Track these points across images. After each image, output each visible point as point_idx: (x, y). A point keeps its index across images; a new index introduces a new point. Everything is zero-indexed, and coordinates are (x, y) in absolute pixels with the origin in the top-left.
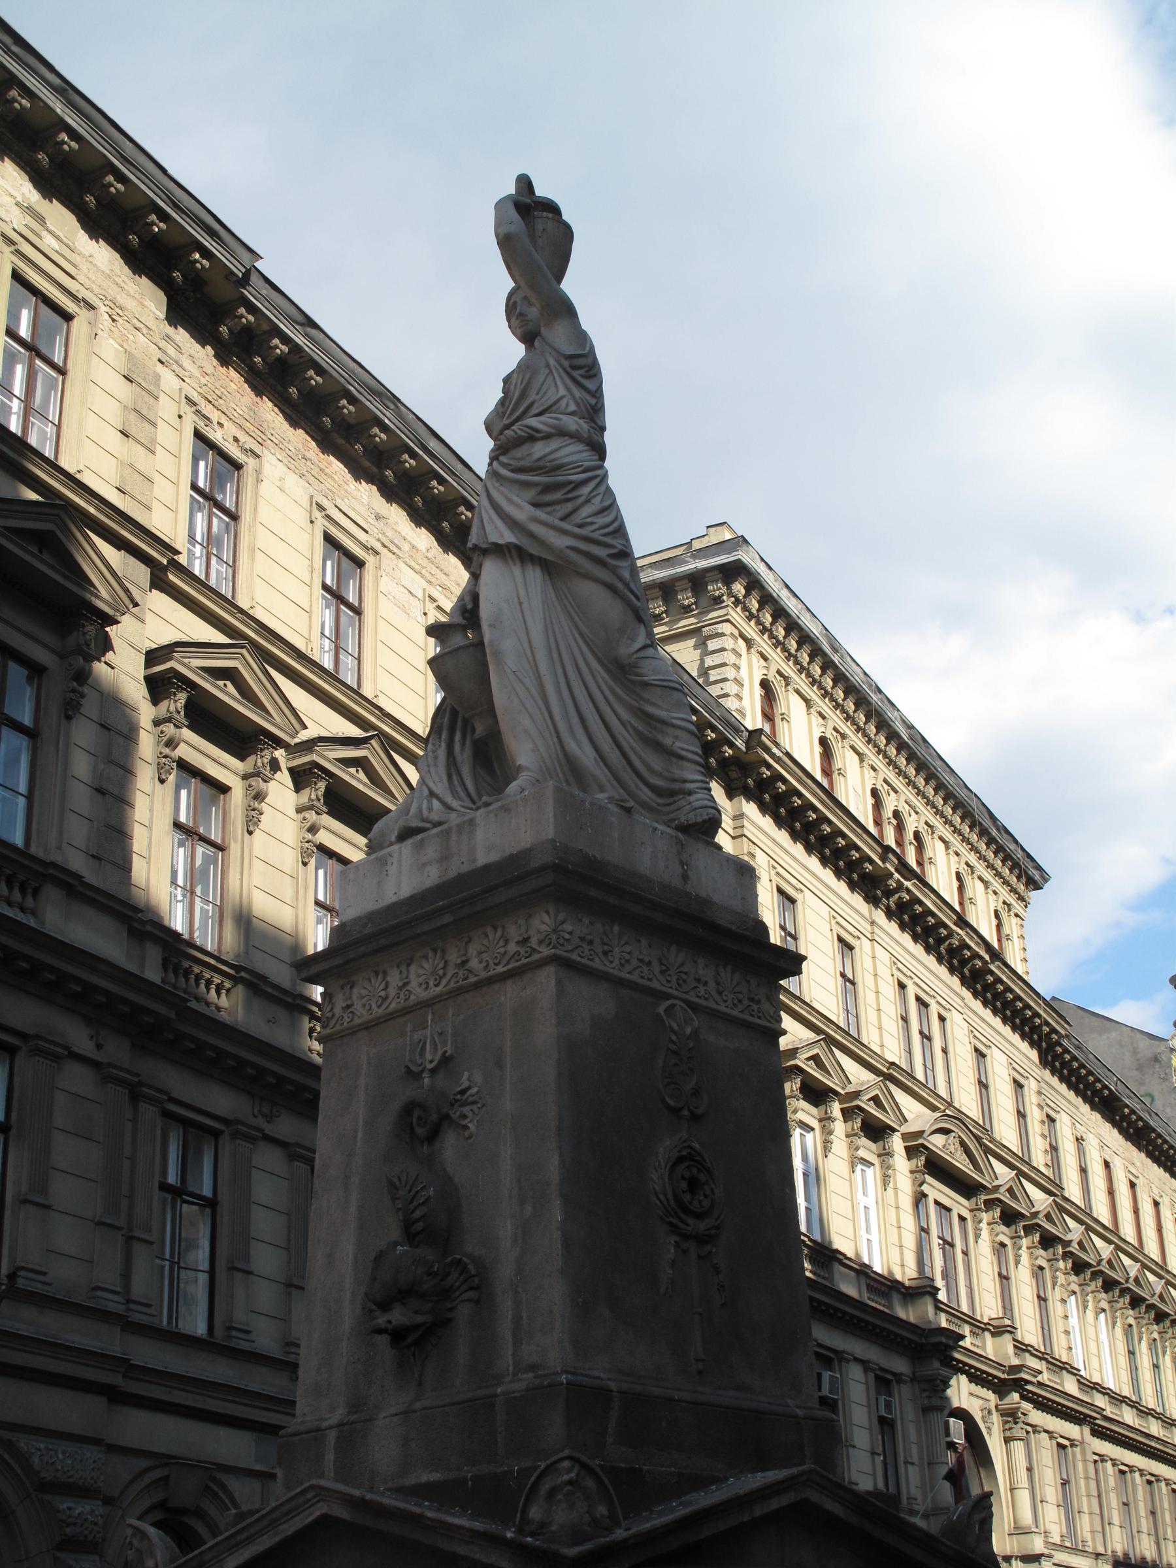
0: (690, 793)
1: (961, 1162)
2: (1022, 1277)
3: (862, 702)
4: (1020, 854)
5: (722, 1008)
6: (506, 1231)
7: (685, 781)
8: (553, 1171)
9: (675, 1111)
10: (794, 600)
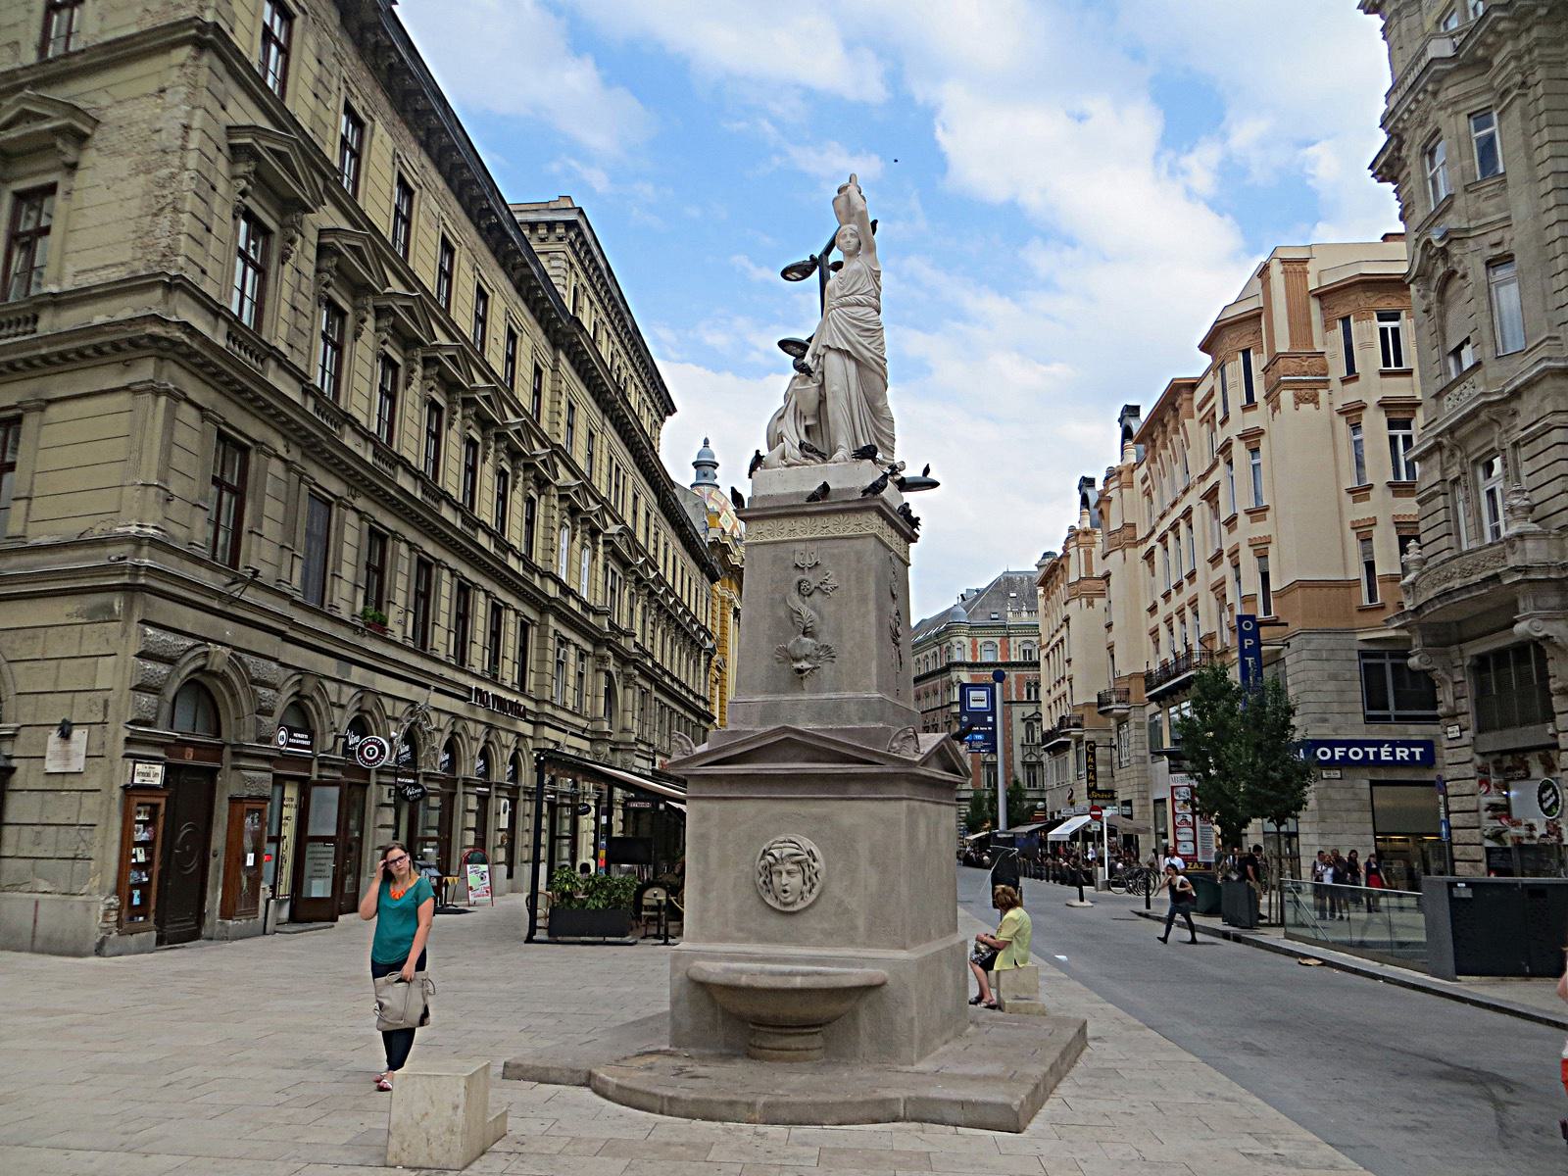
2: (516, 500)
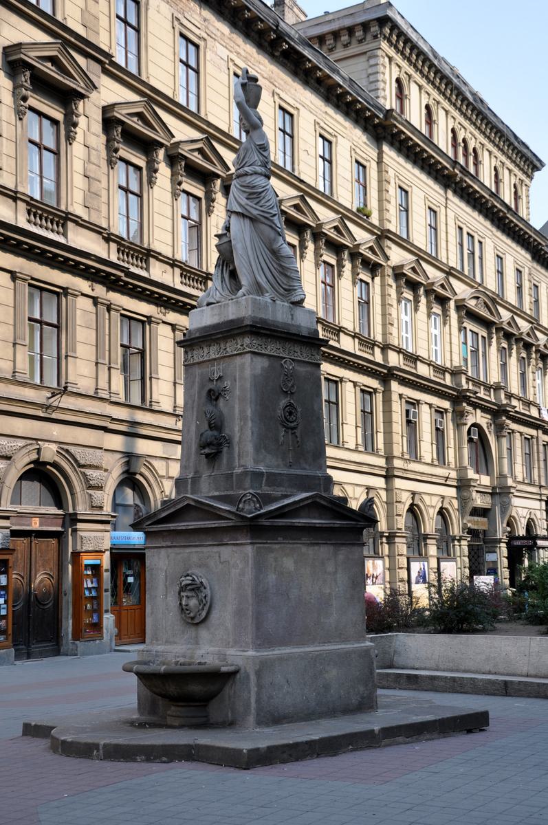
0: (295, 290)
1: (484, 313)
3: (449, 82)
4: (529, 155)
5: (303, 359)
6: (237, 429)
7: (294, 286)
8: (249, 413)
9: (286, 392)
10: (415, 33)
